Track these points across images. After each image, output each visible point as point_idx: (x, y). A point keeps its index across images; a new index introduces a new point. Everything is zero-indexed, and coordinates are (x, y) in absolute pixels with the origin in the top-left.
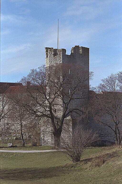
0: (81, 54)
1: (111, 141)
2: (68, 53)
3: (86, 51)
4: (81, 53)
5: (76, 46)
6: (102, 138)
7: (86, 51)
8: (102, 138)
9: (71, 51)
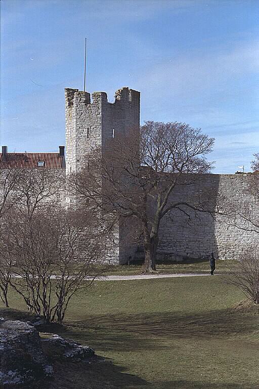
0: (129, 101)
1: (180, 254)
2: (111, 100)
3: (136, 95)
4: (130, 100)
5: (124, 88)
6: (163, 249)
7: (136, 95)
8: (163, 249)
9: (116, 97)
